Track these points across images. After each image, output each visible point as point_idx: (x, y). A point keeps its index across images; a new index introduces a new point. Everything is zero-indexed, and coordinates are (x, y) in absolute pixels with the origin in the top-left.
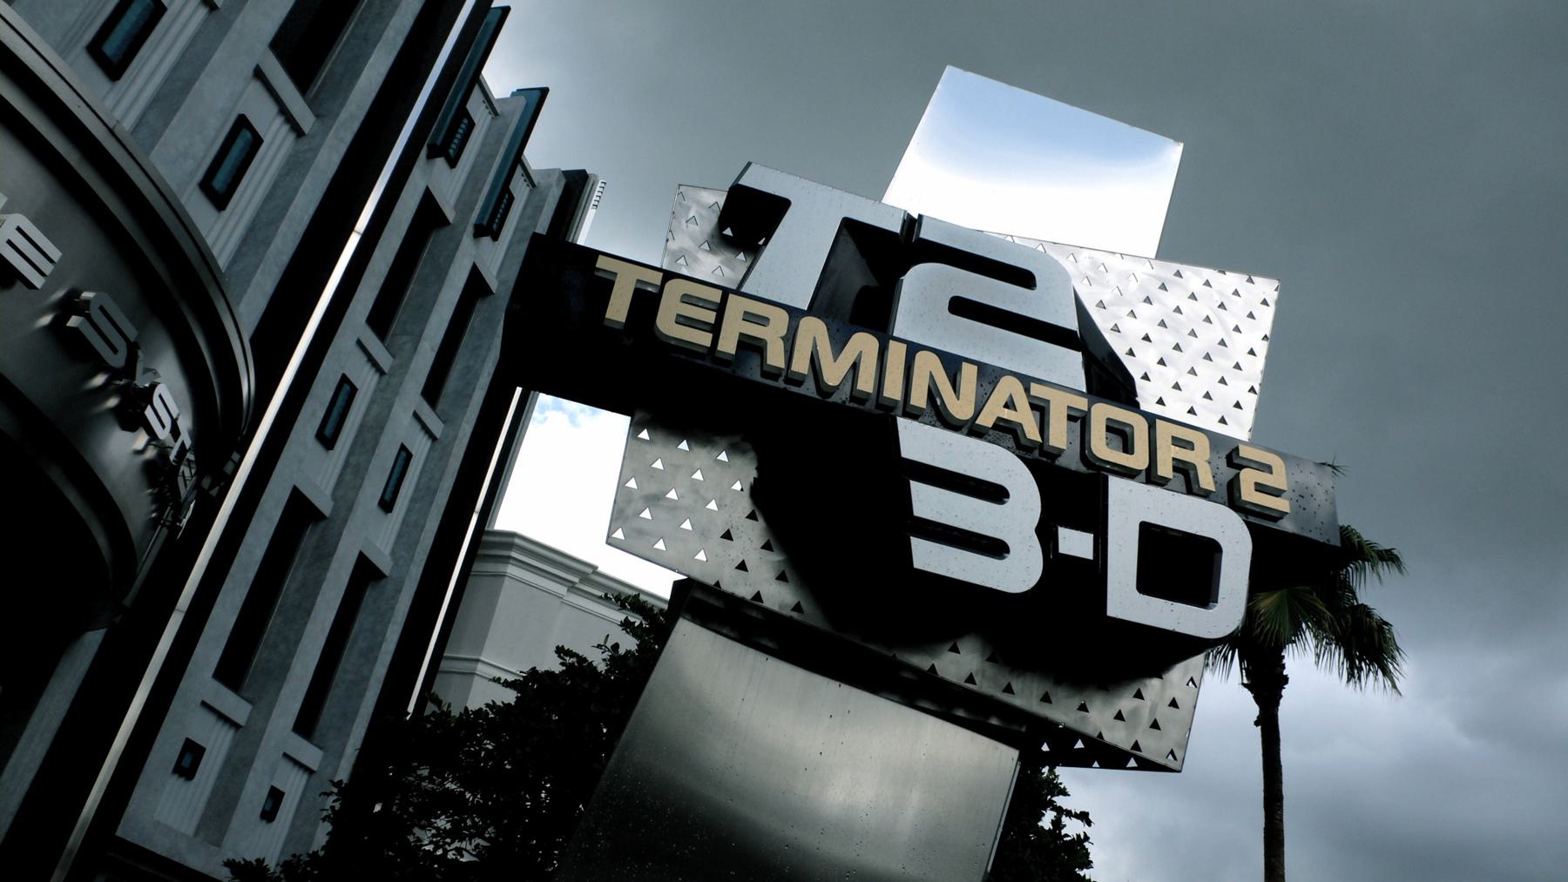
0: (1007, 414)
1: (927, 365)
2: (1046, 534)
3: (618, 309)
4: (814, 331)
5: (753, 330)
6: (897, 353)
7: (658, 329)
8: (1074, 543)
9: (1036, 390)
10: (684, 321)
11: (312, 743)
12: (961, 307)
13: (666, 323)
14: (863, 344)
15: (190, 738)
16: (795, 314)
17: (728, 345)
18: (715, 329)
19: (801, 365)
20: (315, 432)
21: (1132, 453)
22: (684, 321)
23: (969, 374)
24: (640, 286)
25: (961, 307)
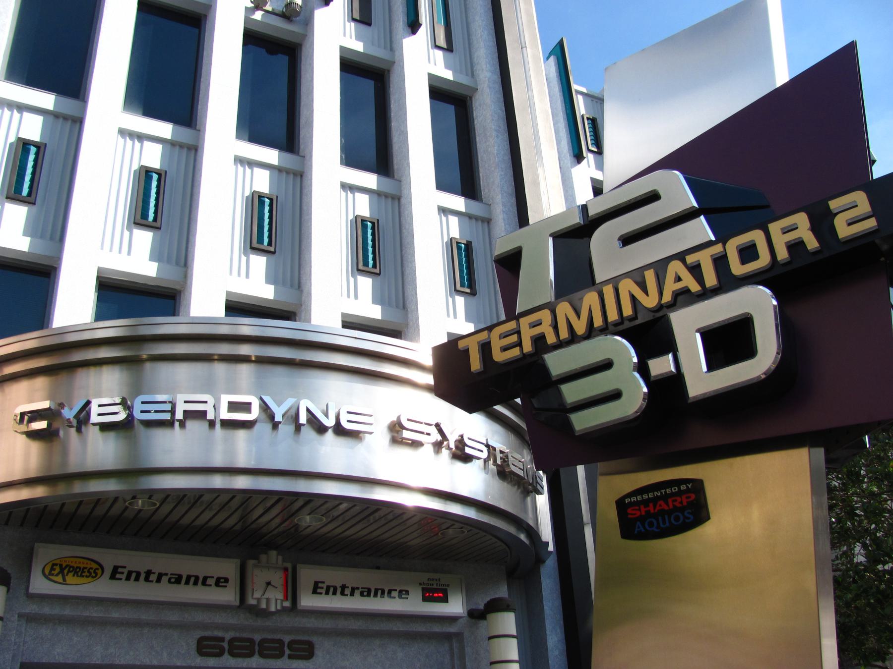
0: (679, 286)
1: (628, 287)
2: (643, 369)
3: (476, 364)
4: (564, 309)
5: (792, 236)
6: (608, 291)
7: (655, 307)
8: (662, 365)
9: (691, 259)
10: (505, 349)
11: (59, 259)
12: (628, 240)
13: (499, 356)
14: (590, 299)
15: (101, 266)
16: (551, 308)
17: (528, 347)
18: (519, 344)
19: (628, 311)
20: (617, 499)
21: (543, 333)
22: (505, 349)
23: (650, 276)
24: (713, 258)
25: (628, 240)
